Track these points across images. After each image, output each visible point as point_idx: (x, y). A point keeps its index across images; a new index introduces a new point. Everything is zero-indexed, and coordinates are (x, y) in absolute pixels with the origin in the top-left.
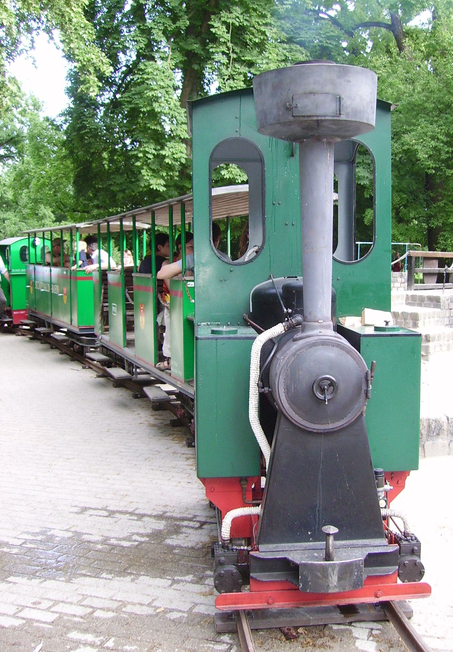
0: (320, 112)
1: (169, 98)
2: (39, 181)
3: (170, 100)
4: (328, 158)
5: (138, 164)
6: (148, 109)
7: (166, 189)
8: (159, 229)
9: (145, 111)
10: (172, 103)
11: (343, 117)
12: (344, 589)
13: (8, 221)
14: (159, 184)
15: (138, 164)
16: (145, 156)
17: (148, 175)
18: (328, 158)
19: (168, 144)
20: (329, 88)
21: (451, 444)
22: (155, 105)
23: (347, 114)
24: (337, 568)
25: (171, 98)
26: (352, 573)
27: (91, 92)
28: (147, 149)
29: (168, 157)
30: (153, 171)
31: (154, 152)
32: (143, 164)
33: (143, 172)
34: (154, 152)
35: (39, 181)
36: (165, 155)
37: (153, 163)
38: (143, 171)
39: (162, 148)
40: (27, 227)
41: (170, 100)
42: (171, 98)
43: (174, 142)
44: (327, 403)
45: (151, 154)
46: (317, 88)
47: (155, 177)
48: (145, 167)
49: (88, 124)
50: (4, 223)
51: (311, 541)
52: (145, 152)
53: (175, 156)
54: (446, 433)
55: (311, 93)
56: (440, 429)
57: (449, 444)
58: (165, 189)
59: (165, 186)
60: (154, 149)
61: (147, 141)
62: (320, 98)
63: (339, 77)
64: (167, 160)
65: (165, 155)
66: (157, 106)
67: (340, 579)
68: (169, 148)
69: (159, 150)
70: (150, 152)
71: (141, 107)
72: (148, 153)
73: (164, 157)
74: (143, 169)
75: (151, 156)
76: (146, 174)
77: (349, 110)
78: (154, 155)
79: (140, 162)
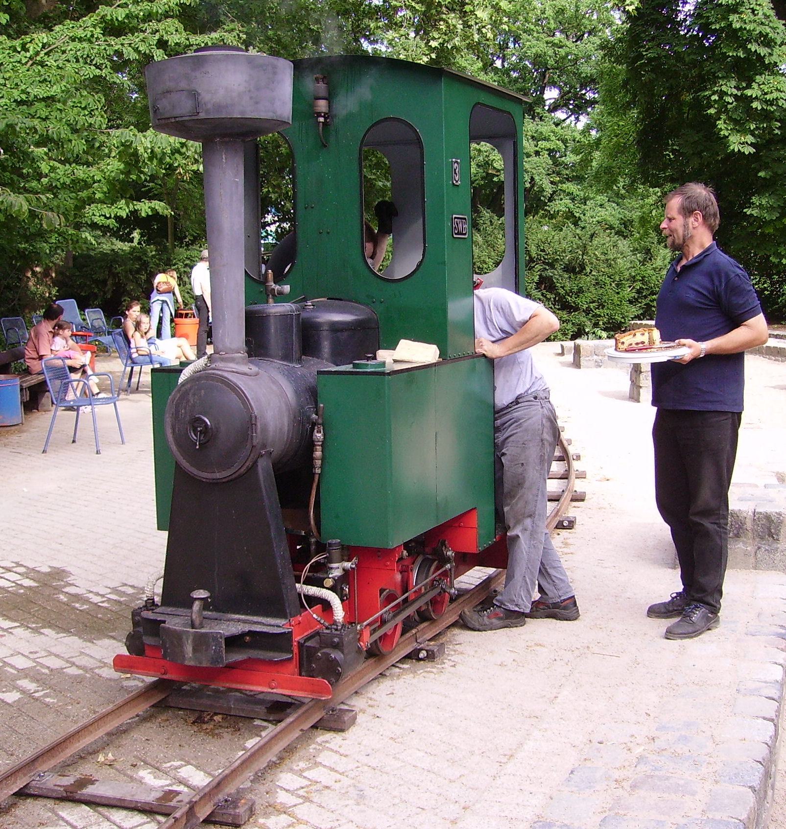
0: (178, 112)
1: (756, 4)
2: (610, 141)
3: (758, 8)
4: (224, 161)
5: (712, 111)
6: (722, 25)
7: (754, 150)
8: (753, 212)
9: (718, 28)
10: (761, 13)
11: (202, 116)
12: (200, 663)
13: (592, 201)
14: (743, 143)
15: (712, 111)
16: (721, 98)
17: (727, 129)
18: (224, 161)
19: (758, 78)
20: (183, 85)
21: (758, 552)
22: (733, 18)
23: (207, 112)
24: (191, 637)
25: (760, 5)
26: (208, 646)
27: (628, 5)
28: (724, 88)
29: (756, 98)
30: (735, 122)
31: (735, 92)
32: (719, 112)
33: (720, 124)
34: (735, 92)
35: (610, 141)
36: (752, 96)
37: (736, 108)
38: (720, 122)
39: (749, 86)
40: (620, 210)
41: (758, 8)
42: (760, 5)
43: (768, 75)
44: (197, 447)
45: (730, 96)
46: (170, 85)
47: (738, 131)
48: (723, 117)
49: (646, 51)
50: (585, 205)
51: (211, 611)
52: (722, 94)
53: (768, 97)
54: (750, 535)
55: (167, 92)
56: (740, 527)
57: (756, 552)
58: (752, 150)
59: (752, 145)
60: (735, 87)
61: (725, 75)
62: (174, 97)
63: (193, 70)
64: (755, 105)
65: (752, 96)
66: (735, 20)
67: (195, 650)
68: (759, 85)
69: (744, 88)
70: (729, 93)
71: (712, 23)
72: (726, 94)
73: (751, 99)
74: (719, 119)
75: (729, 99)
76: (723, 128)
77: (209, 106)
78: (736, 96)
79: (715, 108)
